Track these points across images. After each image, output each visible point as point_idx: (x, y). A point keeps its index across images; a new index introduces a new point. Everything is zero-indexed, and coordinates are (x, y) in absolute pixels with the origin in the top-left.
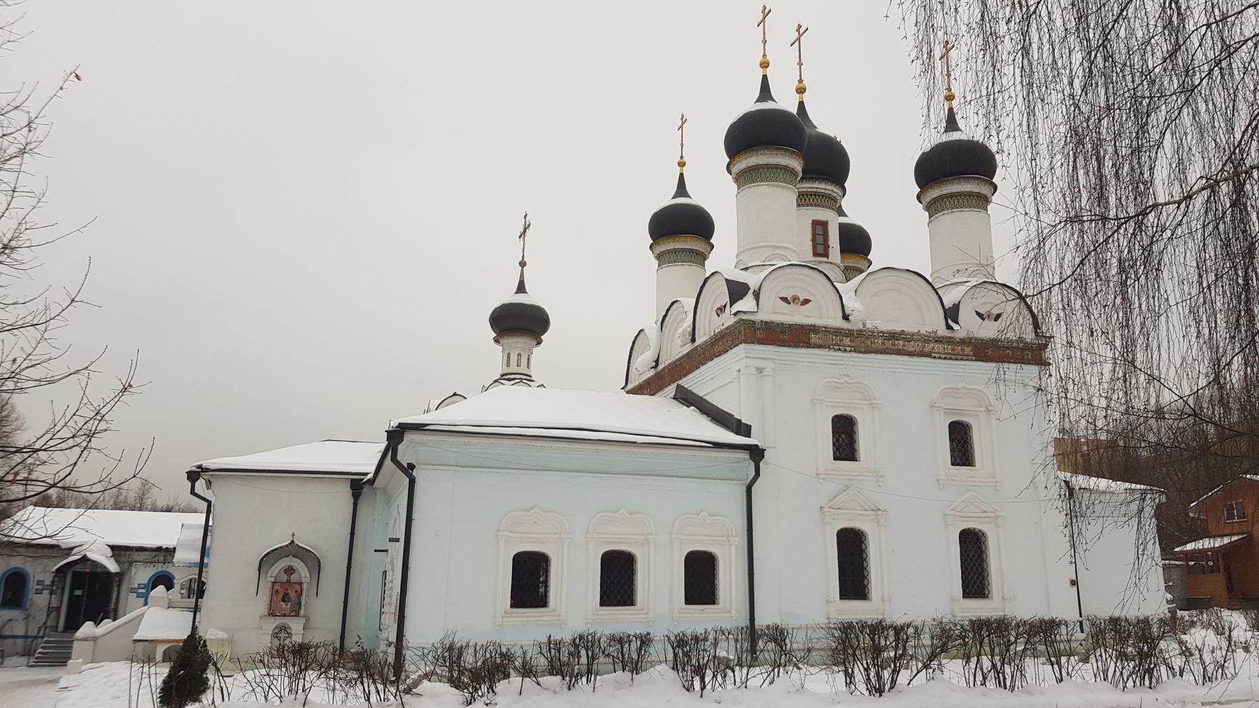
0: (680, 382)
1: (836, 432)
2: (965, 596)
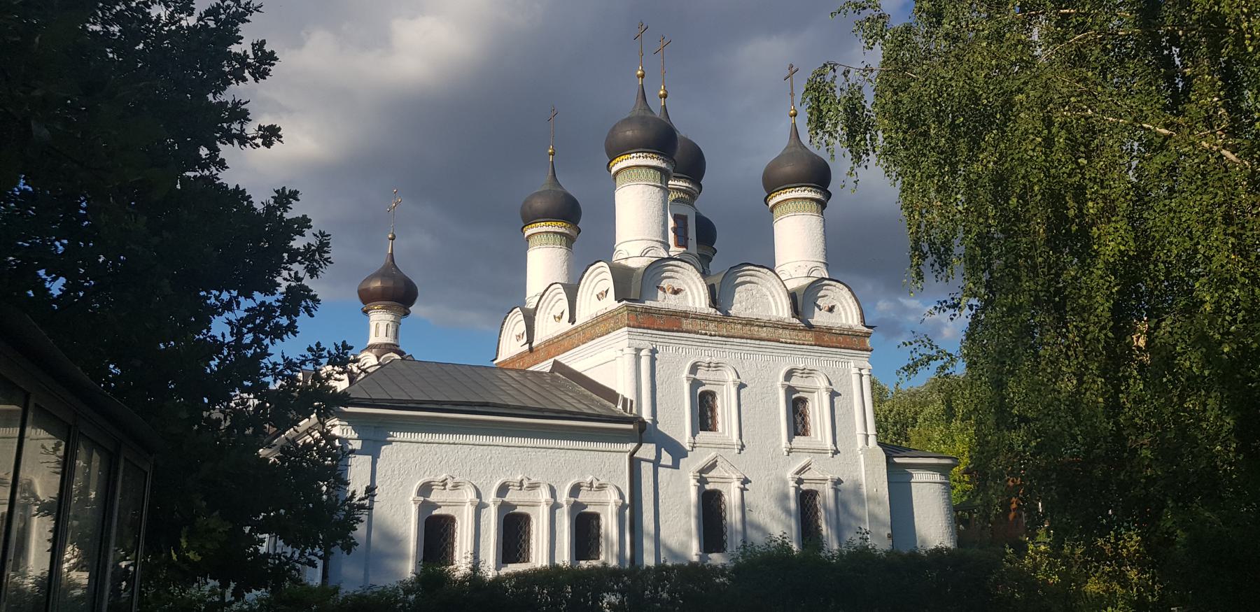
0: (557, 358)
1: (805, 424)
2: (597, 557)
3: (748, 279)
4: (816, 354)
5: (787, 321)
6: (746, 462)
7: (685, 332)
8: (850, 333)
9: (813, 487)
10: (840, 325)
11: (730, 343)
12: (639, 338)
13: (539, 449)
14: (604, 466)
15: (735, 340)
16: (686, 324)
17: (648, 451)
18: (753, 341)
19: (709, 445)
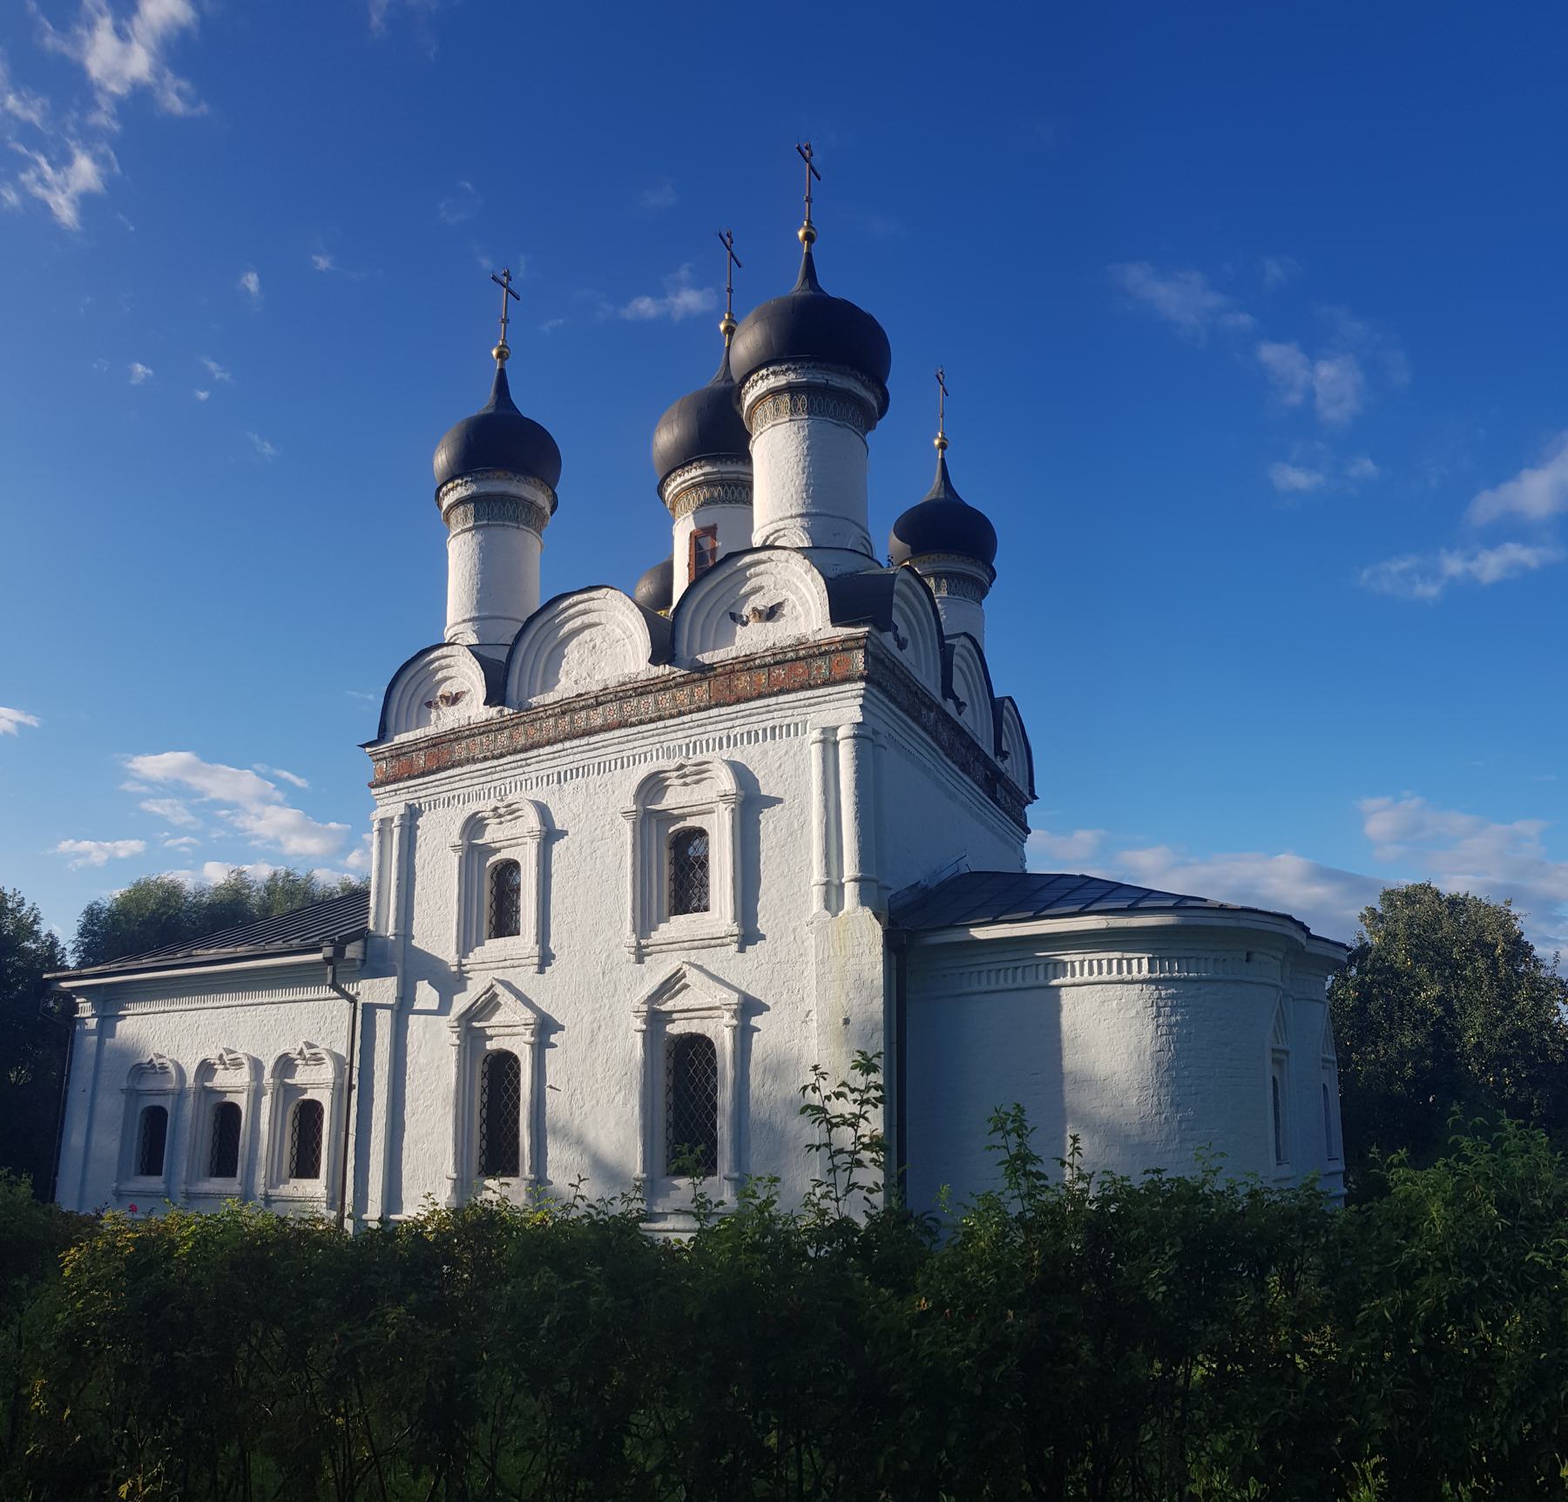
3: (578, 622)
4: (720, 726)
5: (642, 677)
6: (554, 988)
7: (453, 766)
8: (802, 653)
9: (694, 1027)
10: (769, 644)
11: (533, 760)
12: (391, 800)
13: (248, 1008)
14: (324, 1024)
15: (542, 751)
16: (460, 750)
17: (381, 990)
18: (576, 742)
19: (486, 966)
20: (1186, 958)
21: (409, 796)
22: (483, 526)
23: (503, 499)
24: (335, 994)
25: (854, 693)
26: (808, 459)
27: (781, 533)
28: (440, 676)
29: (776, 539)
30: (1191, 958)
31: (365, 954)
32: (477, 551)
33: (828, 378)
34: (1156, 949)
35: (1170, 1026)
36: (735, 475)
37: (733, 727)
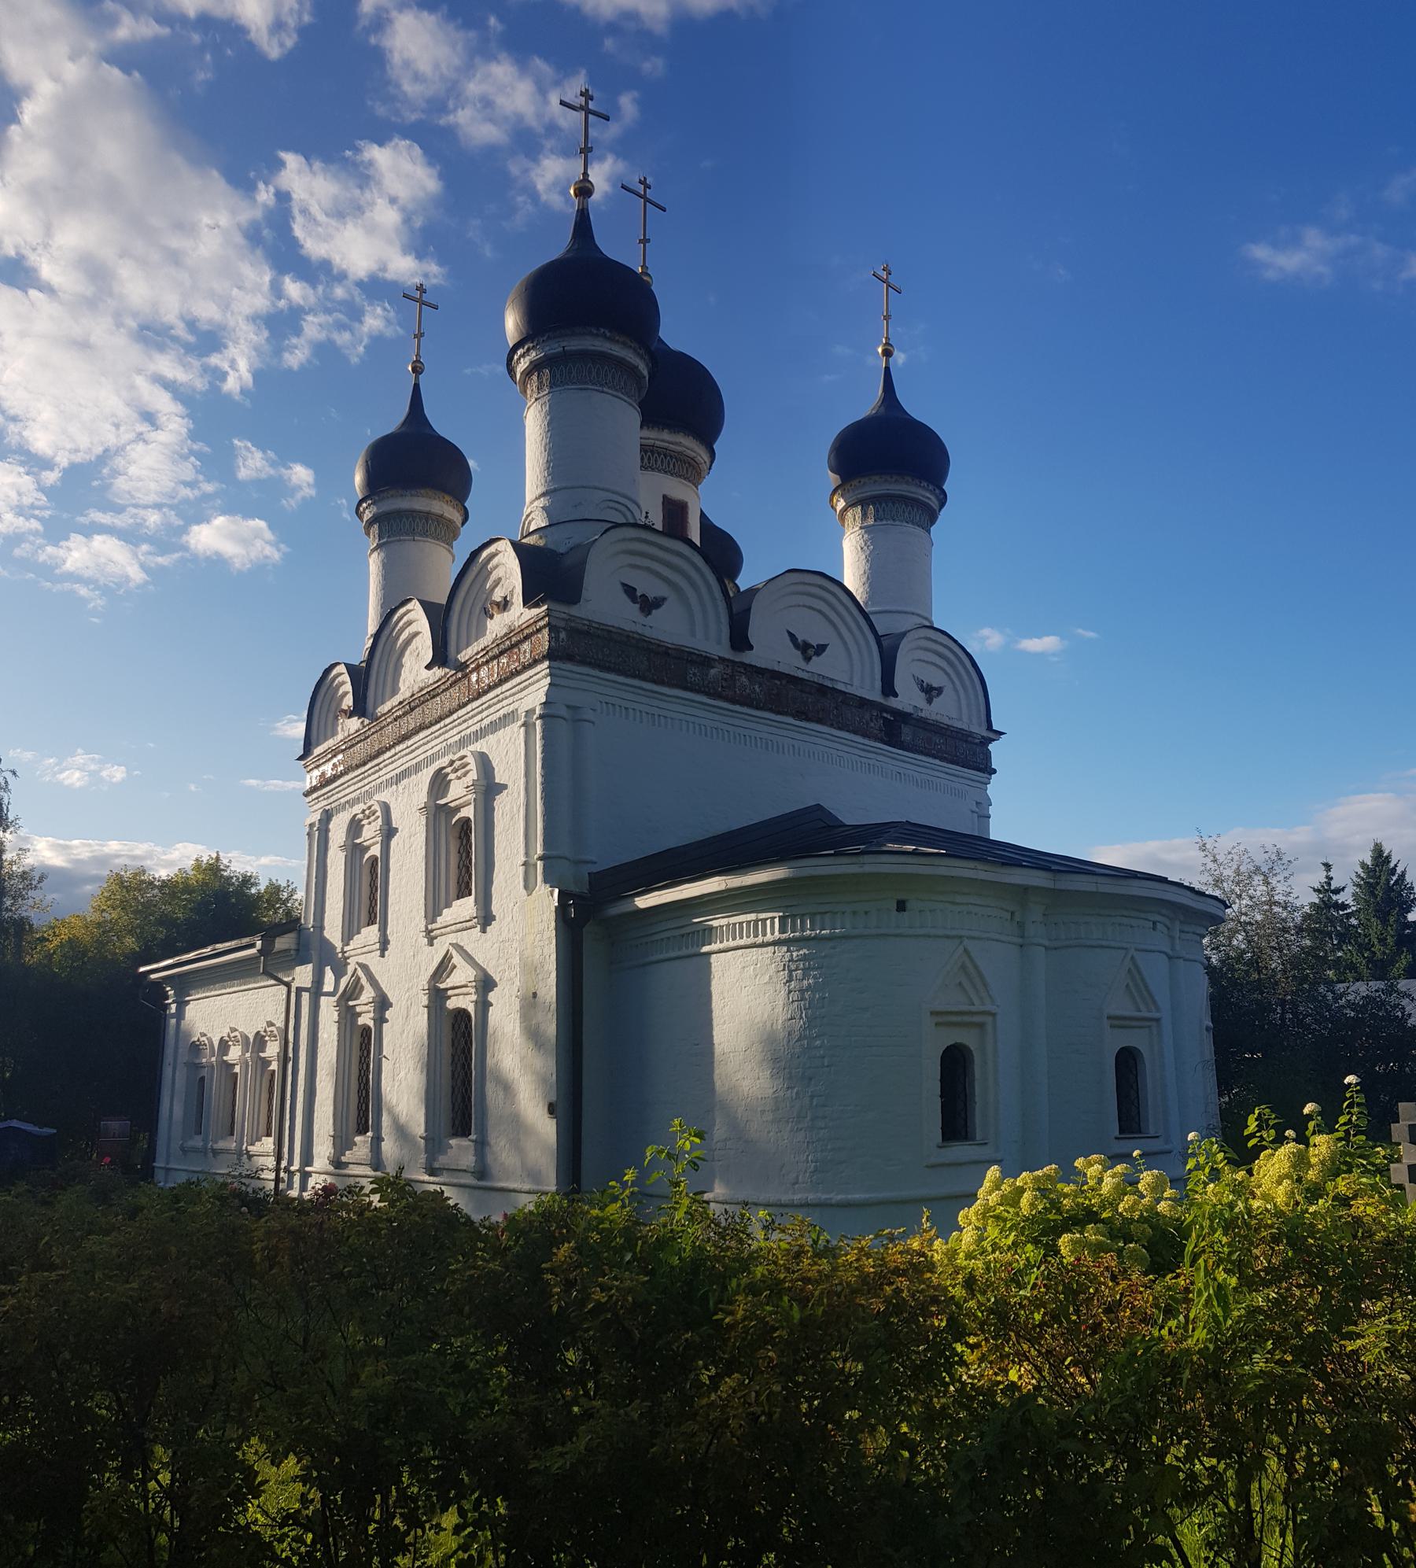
20: (820, 913)
21: (325, 802)
22: (384, 544)
23: (399, 514)
24: (273, 982)
25: (543, 673)
26: (549, 435)
27: (530, 518)
28: (341, 692)
29: (528, 527)
30: (826, 913)
31: (298, 944)
32: (381, 568)
33: (564, 344)
34: (787, 906)
35: (802, 991)
36: (653, 441)
37: (482, 720)
